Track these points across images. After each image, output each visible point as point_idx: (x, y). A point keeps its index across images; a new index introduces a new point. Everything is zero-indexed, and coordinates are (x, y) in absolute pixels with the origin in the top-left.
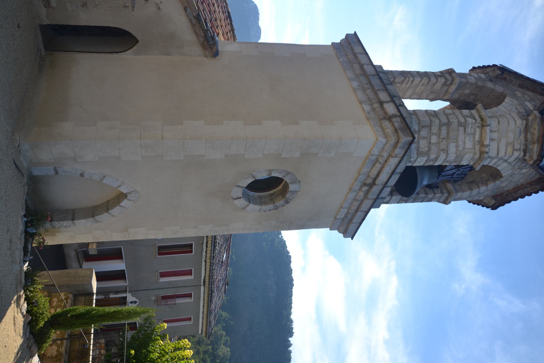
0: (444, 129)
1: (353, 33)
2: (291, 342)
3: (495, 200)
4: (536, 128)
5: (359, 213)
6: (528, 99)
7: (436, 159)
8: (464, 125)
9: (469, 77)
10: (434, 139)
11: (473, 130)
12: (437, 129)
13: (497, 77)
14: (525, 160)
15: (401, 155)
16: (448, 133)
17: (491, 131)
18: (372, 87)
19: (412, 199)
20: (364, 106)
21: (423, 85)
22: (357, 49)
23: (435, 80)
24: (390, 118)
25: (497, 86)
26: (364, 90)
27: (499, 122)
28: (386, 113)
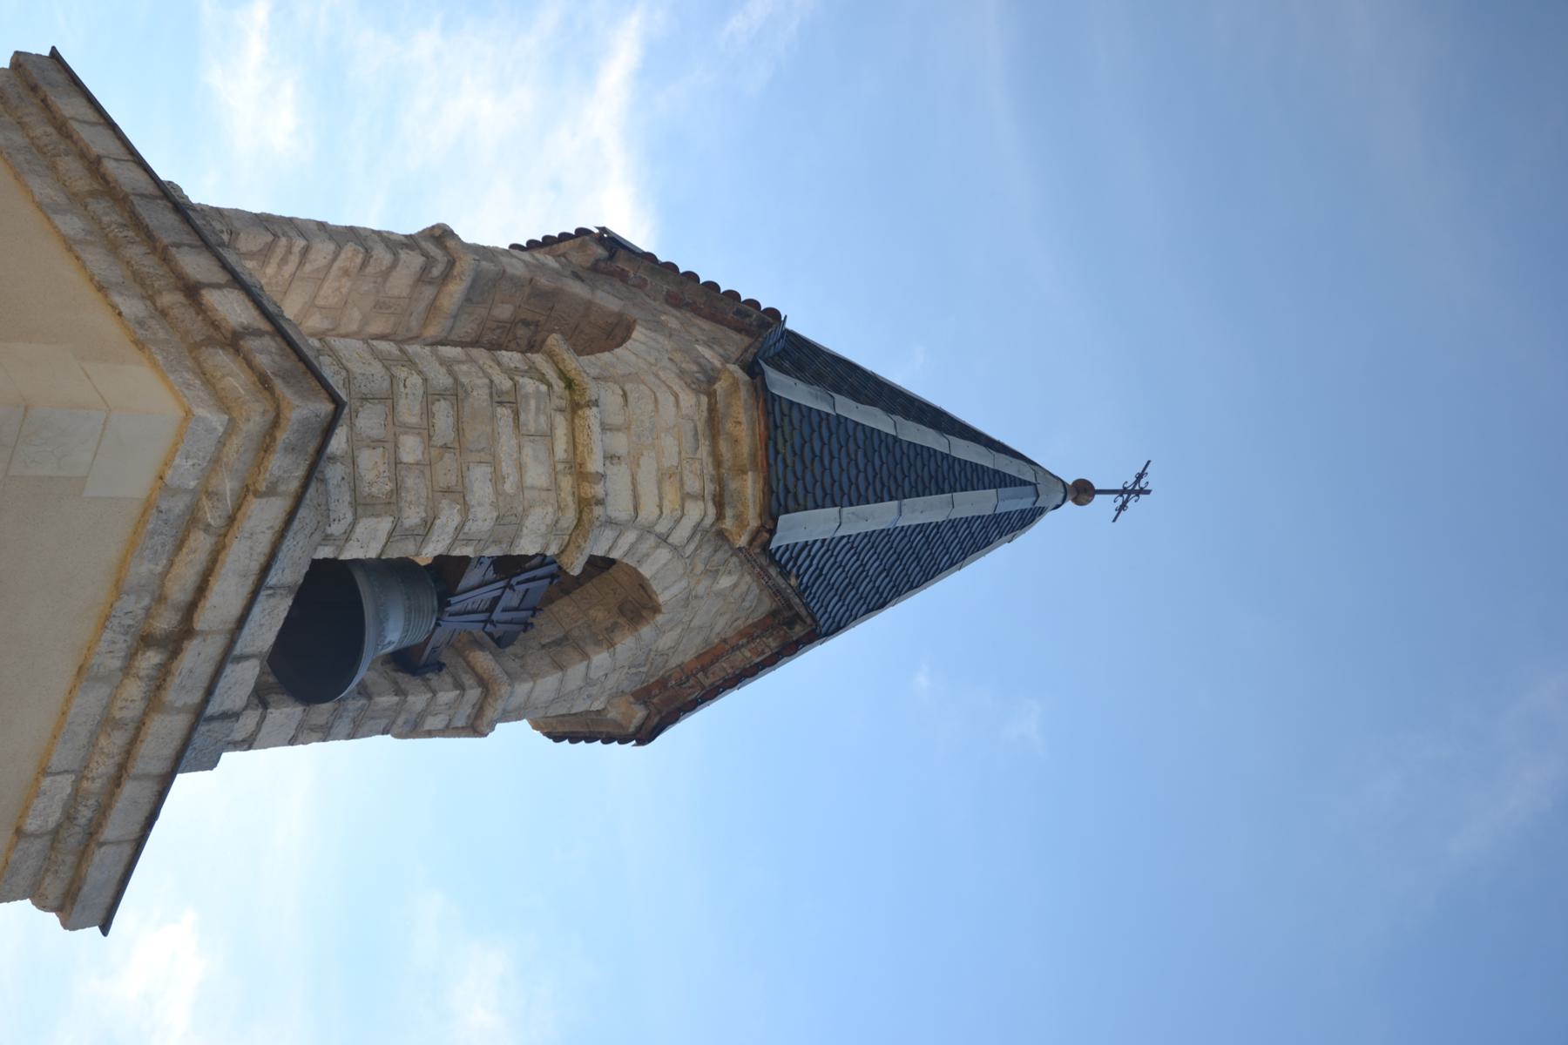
0: (442, 410)
1: (46, 53)
3: (645, 703)
4: (743, 418)
5: (129, 789)
6: (700, 337)
7: (428, 525)
8: (511, 401)
9: (504, 259)
10: (411, 448)
11: (542, 419)
12: (417, 409)
13: (595, 268)
14: (721, 535)
15: (294, 485)
16: (459, 429)
17: (605, 428)
18: (148, 235)
19: (345, 725)
20: (117, 299)
21: (346, 273)
22: (69, 107)
23: (387, 258)
24: (233, 341)
25: (599, 293)
26: (113, 248)
27: (625, 395)
28: (214, 325)
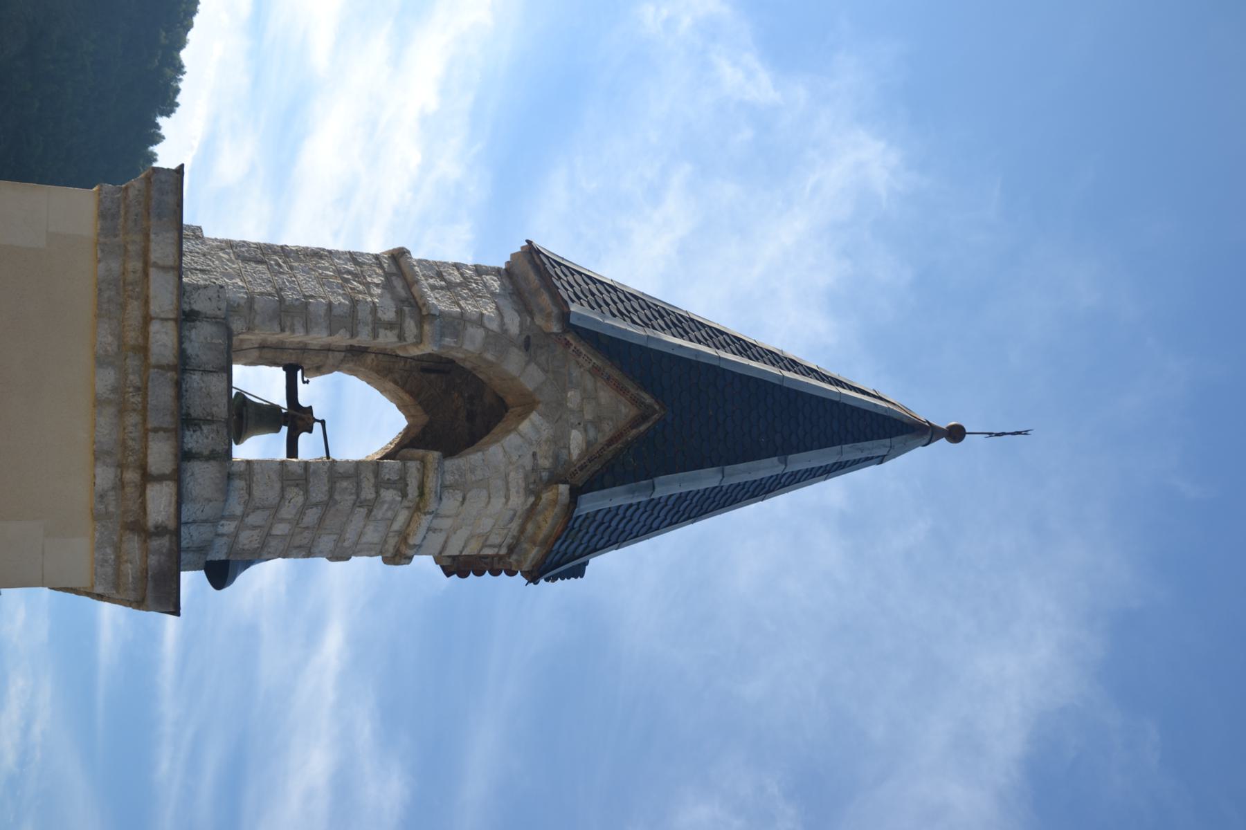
2: (163, 132)
4: (549, 521)
